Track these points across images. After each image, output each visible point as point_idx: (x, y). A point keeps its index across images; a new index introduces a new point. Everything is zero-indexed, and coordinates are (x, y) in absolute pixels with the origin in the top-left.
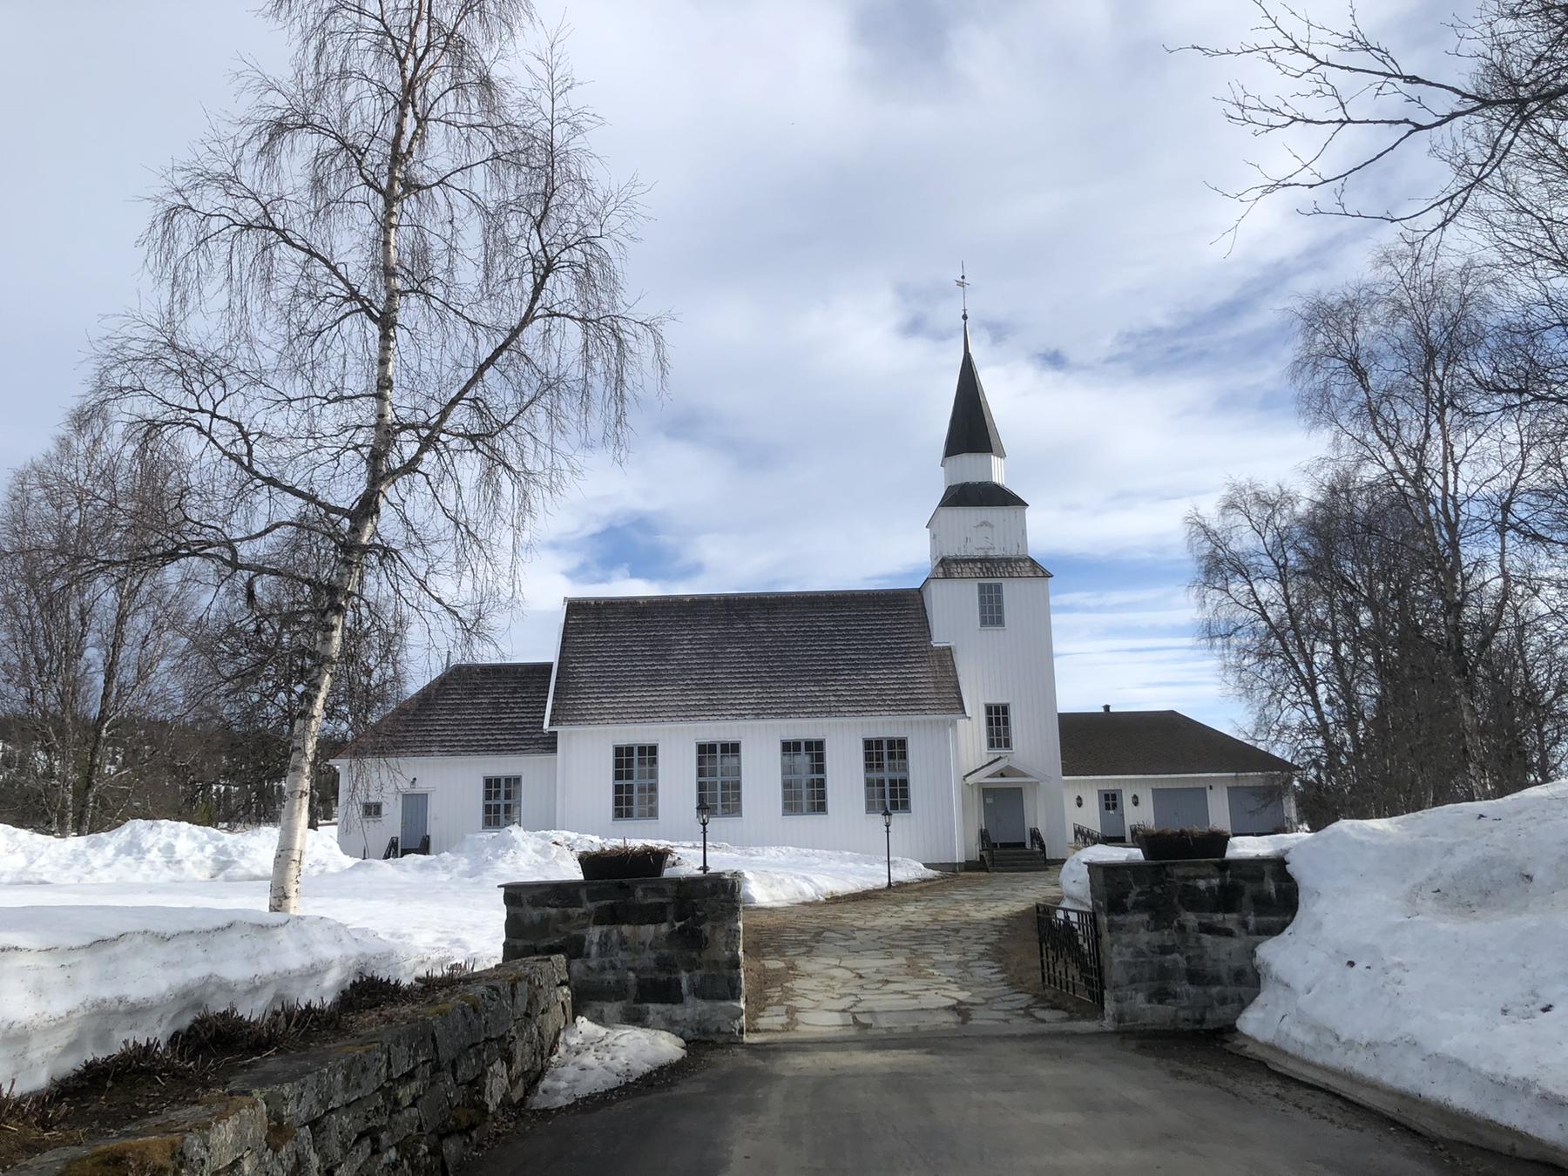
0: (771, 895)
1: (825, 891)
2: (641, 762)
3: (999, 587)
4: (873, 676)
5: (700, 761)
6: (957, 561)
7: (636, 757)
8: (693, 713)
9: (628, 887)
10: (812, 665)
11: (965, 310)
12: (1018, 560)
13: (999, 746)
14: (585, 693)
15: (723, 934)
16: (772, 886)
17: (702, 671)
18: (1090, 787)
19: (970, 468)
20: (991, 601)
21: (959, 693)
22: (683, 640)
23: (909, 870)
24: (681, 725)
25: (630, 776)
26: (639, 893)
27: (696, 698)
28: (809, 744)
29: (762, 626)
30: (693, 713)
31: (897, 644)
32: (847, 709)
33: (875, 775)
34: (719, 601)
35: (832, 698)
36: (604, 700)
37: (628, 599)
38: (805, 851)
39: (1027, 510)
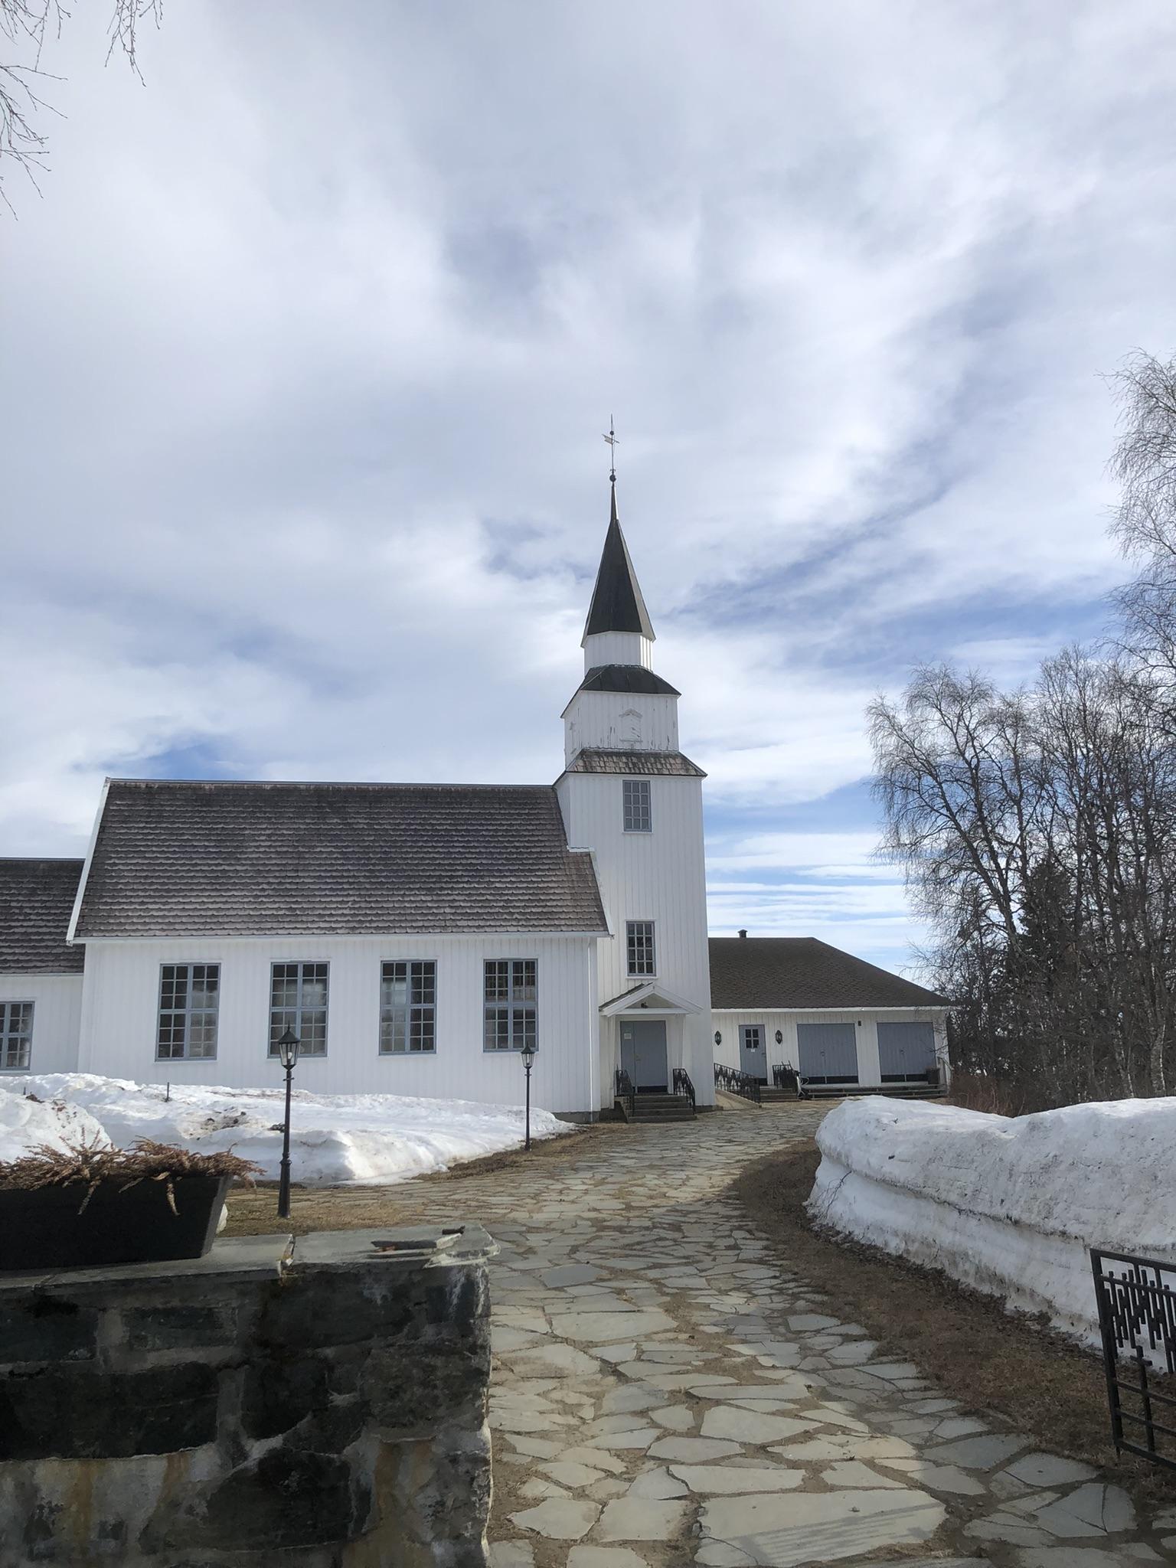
0: (377, 1167)
1: (447, 1157)
2: (197, 985)
3: (646, 786)
4: (498, 885)
5: (276, 985)
6: (600, 754)
7: (190, 979)
8: (269, 926)
9: (71, 1308)
10: (423, 870)
11: (613, 471)
12: (667, 756)
13: (641, 971)
14: (126, 897)
15: (428, 1472)
16: (377, 1152)
17: (283, 874)
18: (730, 1023)
19: (615, 648)
20: (637, 802)
21: (600, 906)
22: (261, 835)
23: (544, 1124)
24: (252, 940)
25: (180, 1004)
26: (113, 1330)
27: (272, 906)
28: (416, 967)
29: (362, 822)
30: (269, 926)
31: (528, 847)
32: (465, 923)
33: (497, 1005)
34: (308, 790)
35: (448, 910)
36: (150, 907)
37: (190, 783)
38: (407, 1100)
39: (679, 700)
